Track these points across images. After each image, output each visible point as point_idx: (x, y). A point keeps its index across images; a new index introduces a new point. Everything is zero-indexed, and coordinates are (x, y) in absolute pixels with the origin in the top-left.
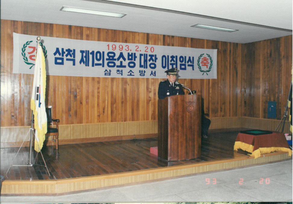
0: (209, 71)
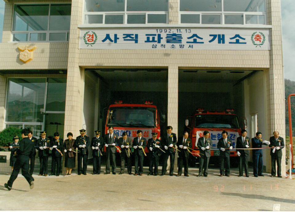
0: (262, 44)
